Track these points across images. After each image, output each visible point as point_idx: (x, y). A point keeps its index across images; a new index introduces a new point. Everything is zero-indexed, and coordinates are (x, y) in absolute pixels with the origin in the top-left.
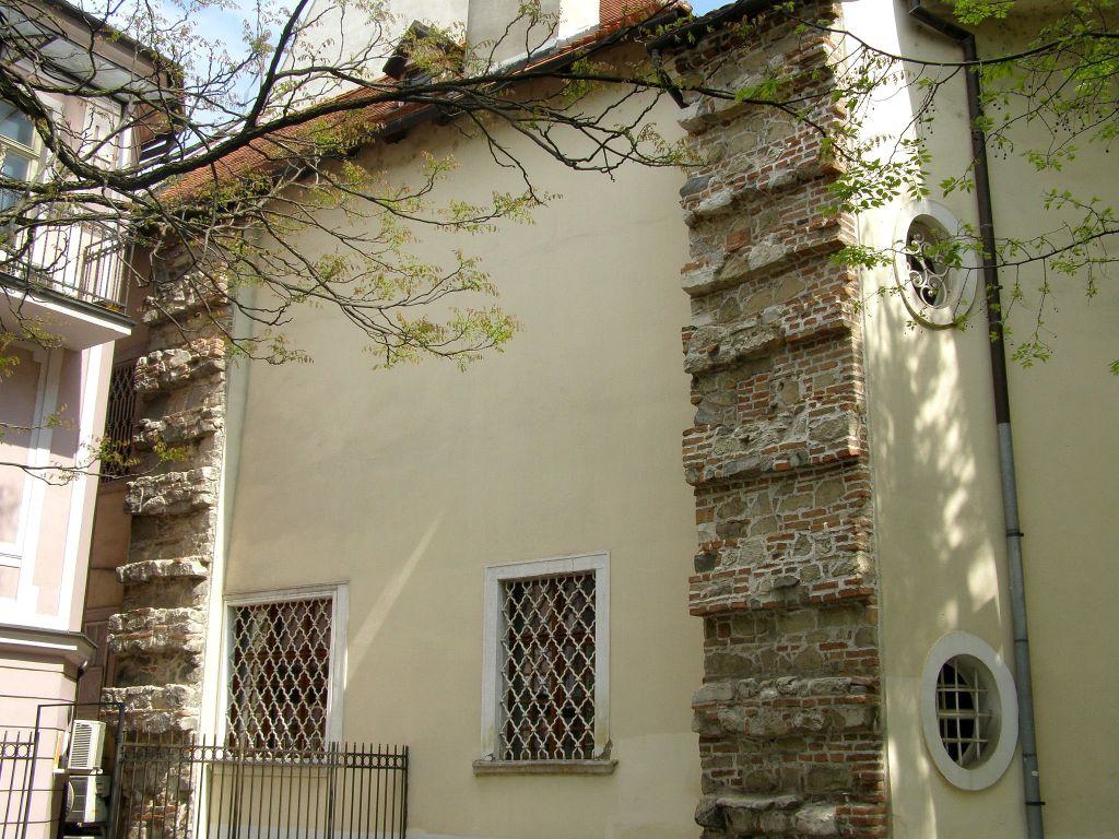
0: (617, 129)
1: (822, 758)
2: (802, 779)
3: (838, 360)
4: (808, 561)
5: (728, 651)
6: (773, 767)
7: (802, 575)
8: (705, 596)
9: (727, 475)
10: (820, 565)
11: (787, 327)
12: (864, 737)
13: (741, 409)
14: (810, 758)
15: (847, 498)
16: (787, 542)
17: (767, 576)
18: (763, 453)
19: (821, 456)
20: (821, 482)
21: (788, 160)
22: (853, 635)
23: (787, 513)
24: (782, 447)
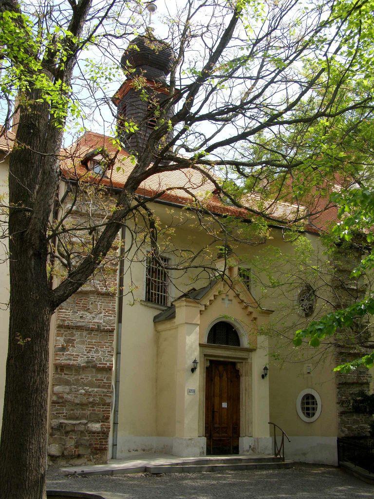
0: (273, 85)
1: (95, 410)
5: (63, 377)
6: (78, 412)
8: (62, 360)
11: (100, 288)
12: (107, 406)
13: (76, 306)
14: (90, 410)
24: (94, 322)
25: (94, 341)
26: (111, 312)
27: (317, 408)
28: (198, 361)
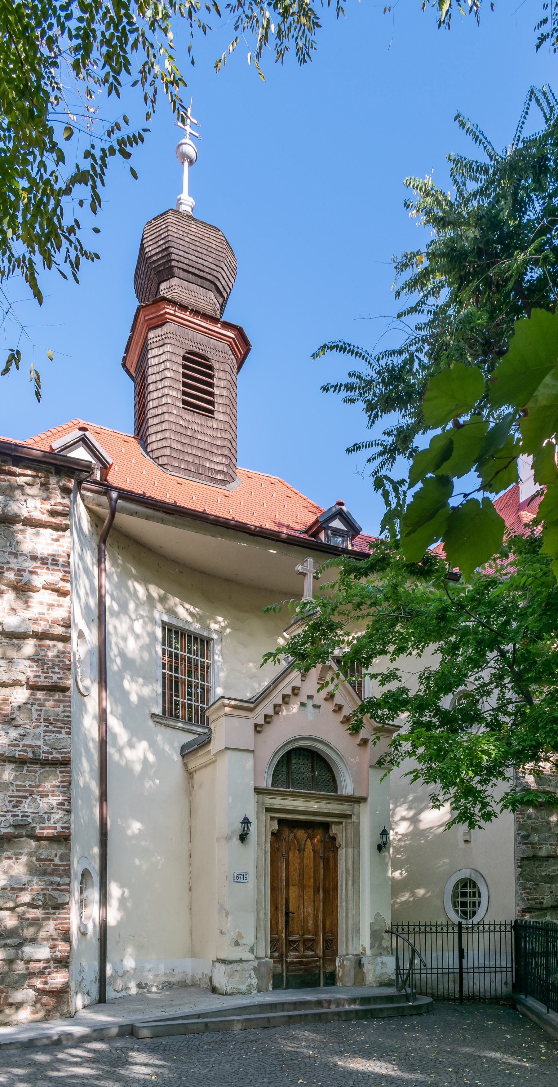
7: (33, 820)
17: (8, 817)
19: (50, 756)
20: (43, 770)
22: (58, 855)
23: (18, 783)
24: (24, 745)
25: (27, 783)
26: (60, 724)
27: (479, 903)
28: (252, 819)
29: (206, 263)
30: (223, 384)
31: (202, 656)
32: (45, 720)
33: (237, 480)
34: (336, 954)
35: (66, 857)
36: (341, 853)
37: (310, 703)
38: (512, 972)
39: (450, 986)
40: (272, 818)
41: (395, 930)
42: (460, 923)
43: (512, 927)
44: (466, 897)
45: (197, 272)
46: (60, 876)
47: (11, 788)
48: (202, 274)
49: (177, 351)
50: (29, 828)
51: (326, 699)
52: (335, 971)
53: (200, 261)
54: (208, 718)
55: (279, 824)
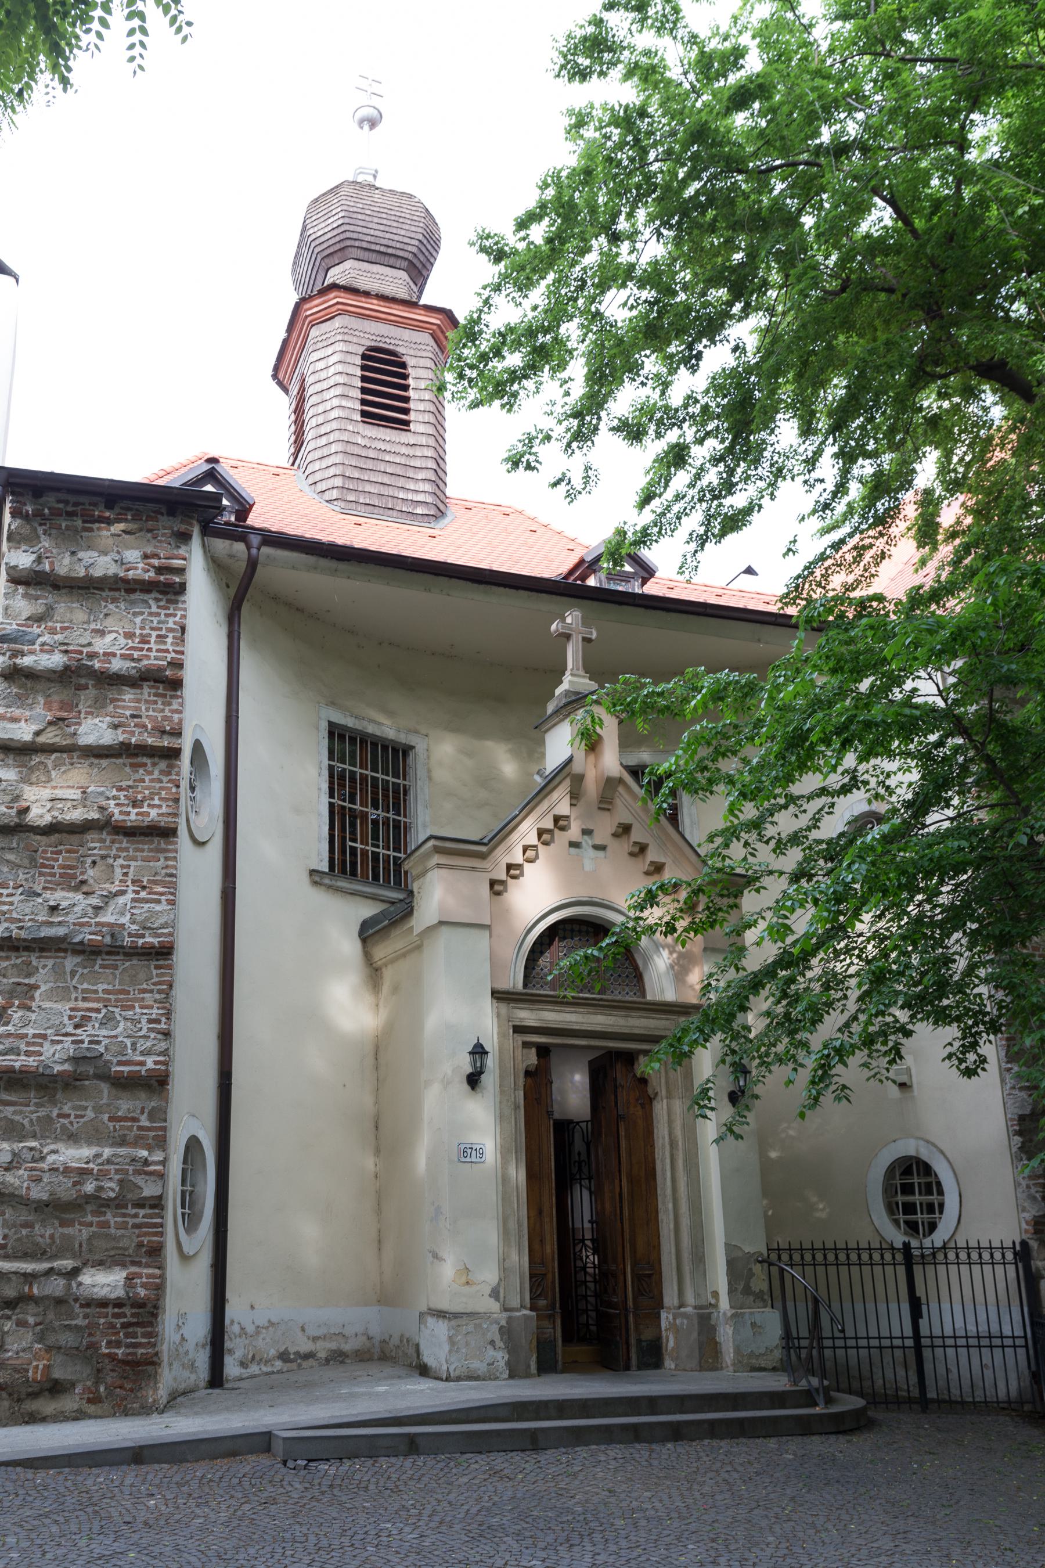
1: (106, 1225)
2: (81, 1245)
3: (161, 856)
4: (115, 1037)
6: (45, 1232)
7: (106, 1049)
9: (30, 937)
10: (128, 1042)
11: (116, 811)
12: (152, 1207)
13: (41, 874)
14: (91, 1225)
15: (154, 984)
16: (94, 1015)
17: (66, 1045)
18: (75, 924)
19: (141, 941)
20: (128, 964)
21: (136, 654)
23: (85, 986)
24: (98, 924)
27: (941, 1206)
29: (396, 238)
30: (421, 407)
31: (396, 775)
32: (134, 882)
33: (448, 513)
34: (660, 1305)
35: (159, 1115)
36: (660, 1108)
37: (587, 842)
38: (1026, 1346)
39: (905, 1379)
40: (526, 1045)
41: (774, 1257)
42: (907, 1246)
43: (1015, 1254)
44: (913, 1193)
45: (382, 249)
46: (150, 1149)
47: (73, 996)
48: (390, 251)
49: (351, 348)
50: (100, 1063)
51: (615, 835)
52: (659, 1338)
53: (388, 236)
54: (406, 873)
55: (539, 1055)
